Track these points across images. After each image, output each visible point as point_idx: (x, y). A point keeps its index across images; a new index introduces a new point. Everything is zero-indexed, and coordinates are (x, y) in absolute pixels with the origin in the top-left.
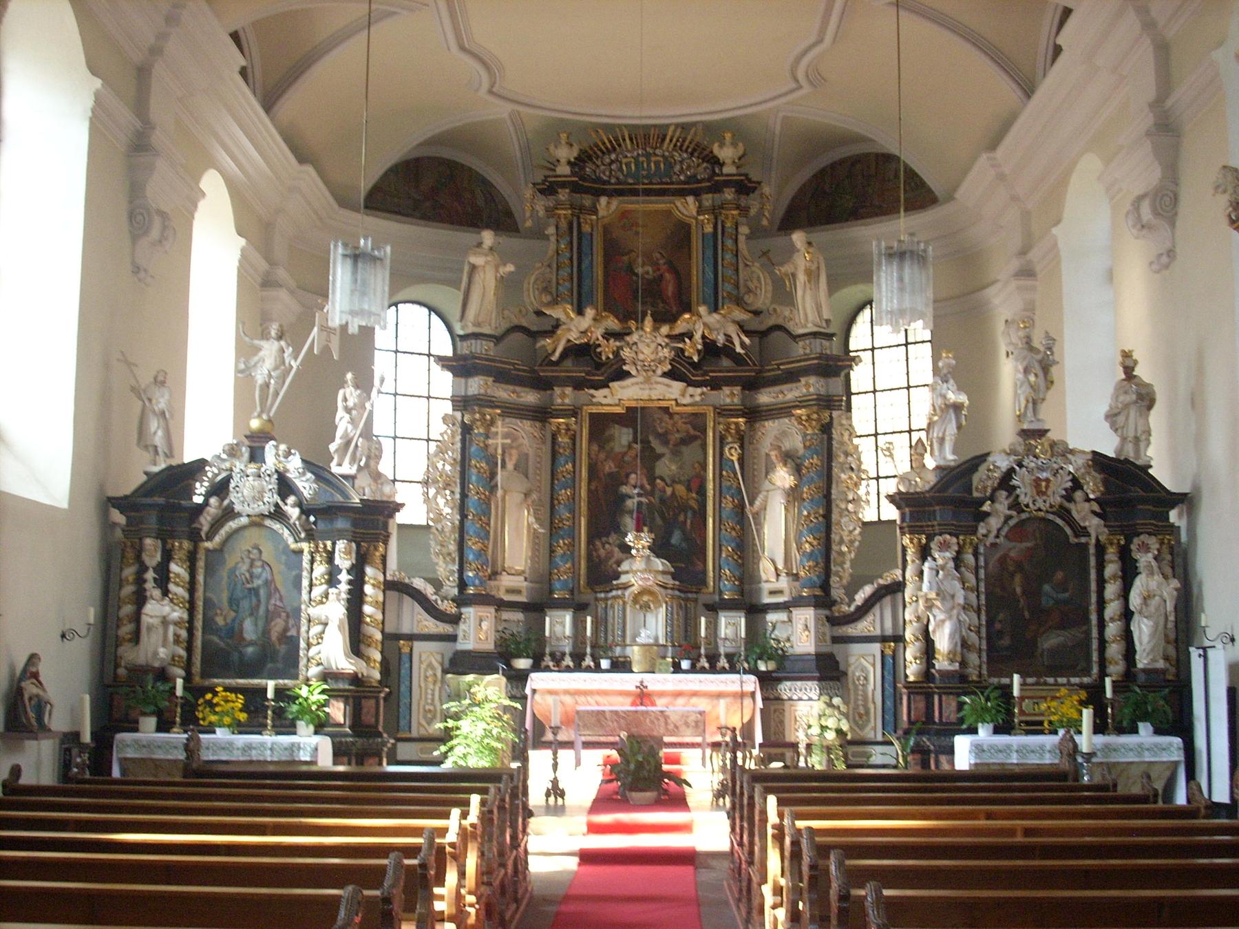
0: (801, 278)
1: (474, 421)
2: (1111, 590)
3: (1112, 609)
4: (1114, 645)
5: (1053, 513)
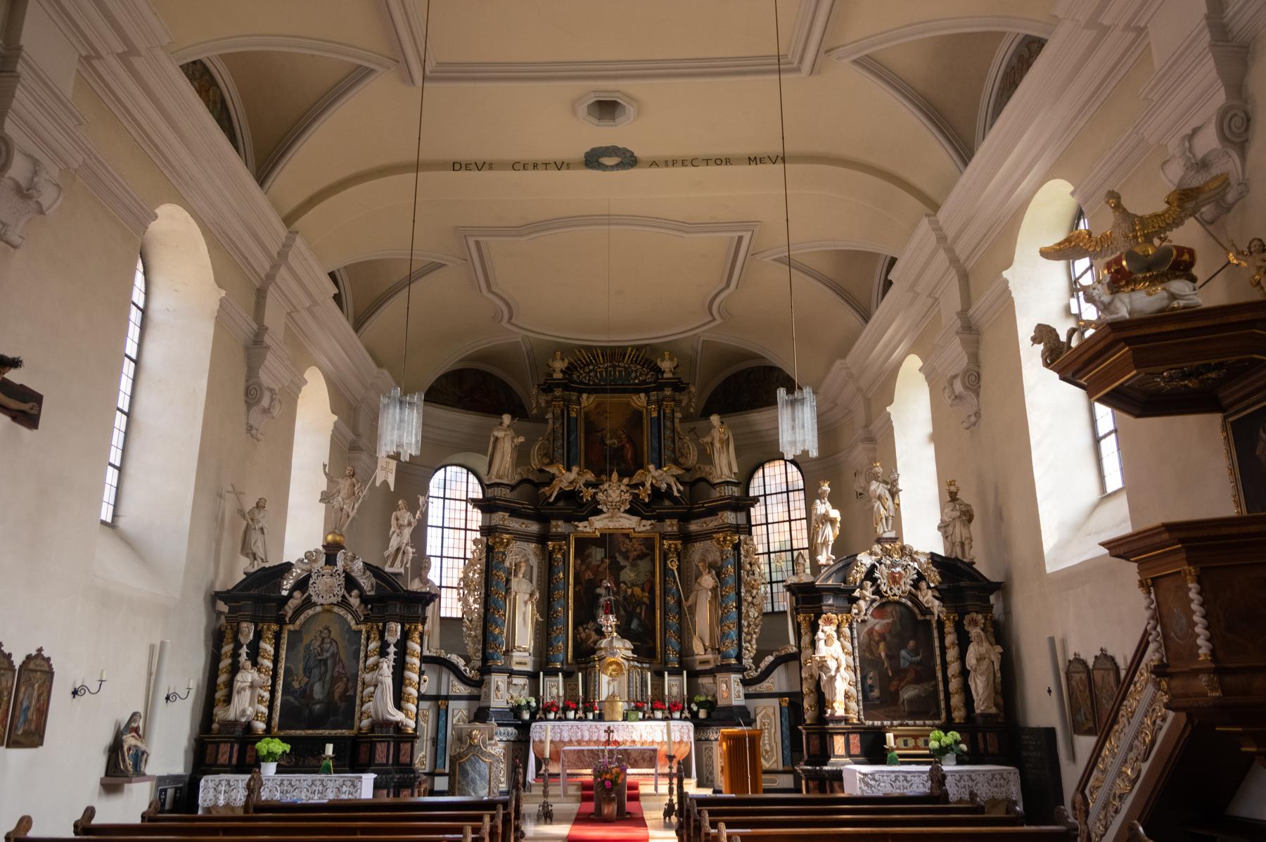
0: (717, 445)
1: (495, 543)
2: (952, 654)
3: (953, 668)
4: (956, 696)
5: (905, 598)
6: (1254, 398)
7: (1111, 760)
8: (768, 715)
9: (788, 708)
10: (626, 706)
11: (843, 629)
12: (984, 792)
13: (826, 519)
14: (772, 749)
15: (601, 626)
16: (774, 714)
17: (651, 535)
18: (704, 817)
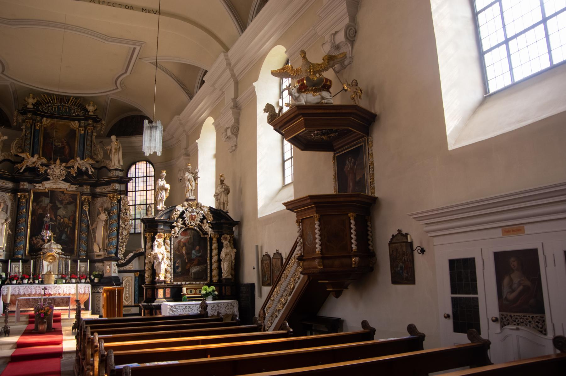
0: (113, 150)
2: (215, 252)
3: (215, 259)
4: (215, 271)
5: (196, 227)
6: (346, 147)
7: (277, 296)
8: (129, 281)
9: (139, 277)
10: (56, 277)
11: (167, 240)
12: (223, 311)
13: (163, 188)
14: (129, 296)
15: (43, 236)
16: (132, 280)
17: (75, 193)
18: (88, 330)
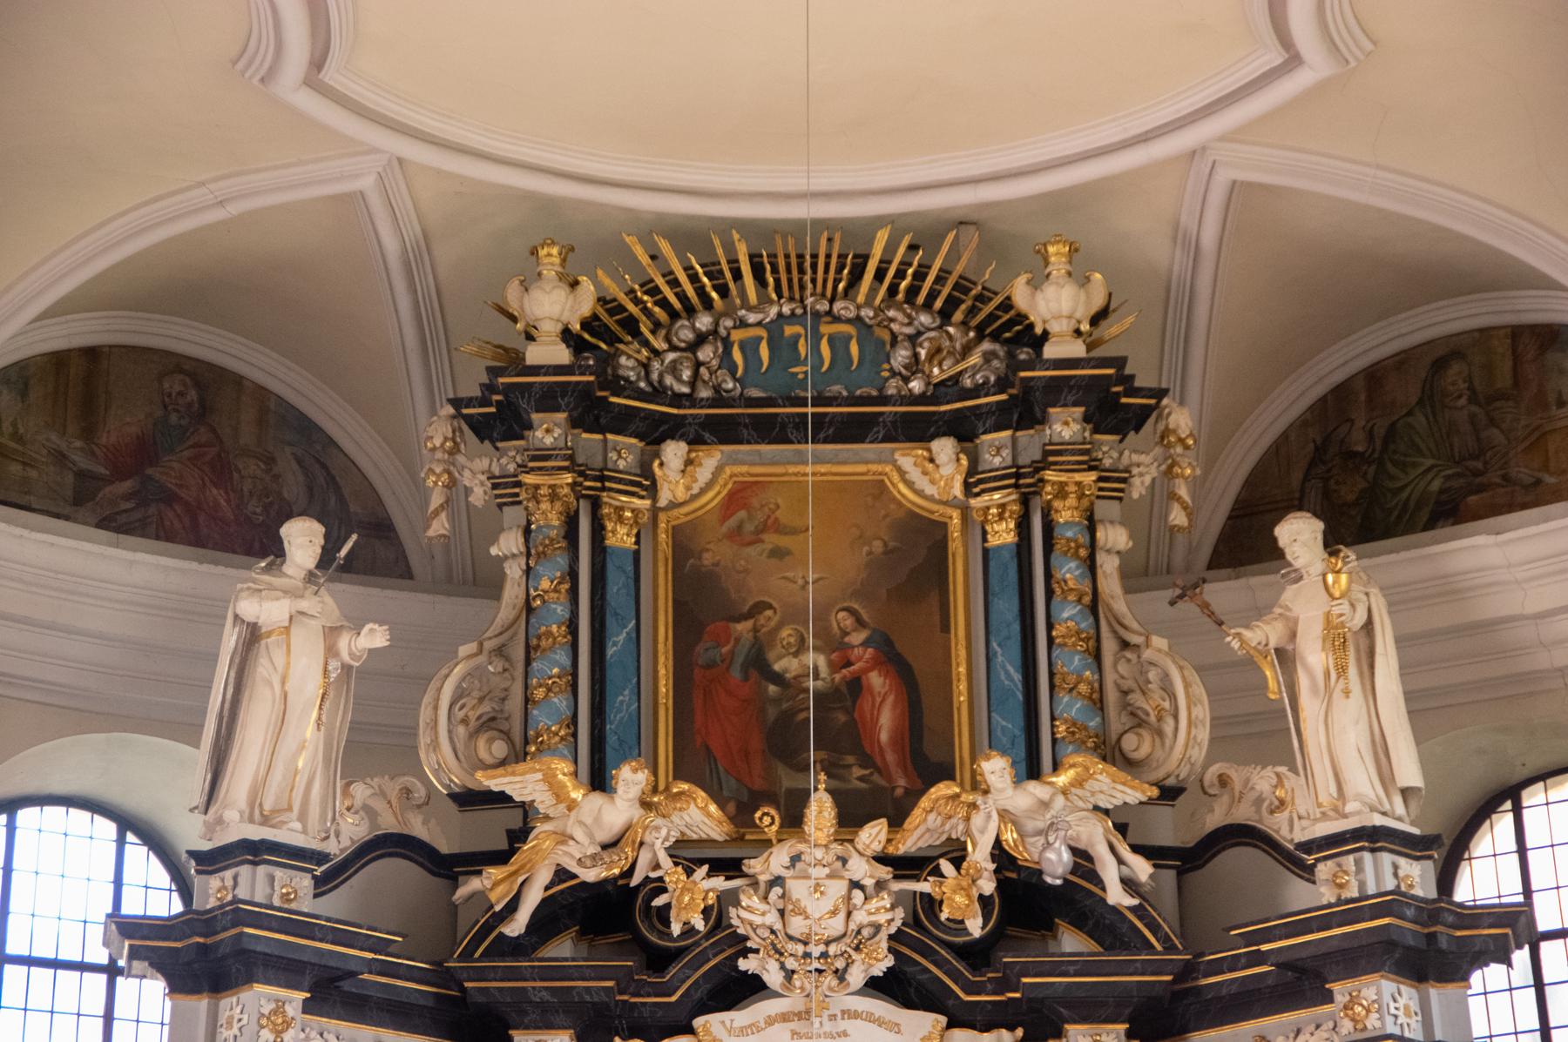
0: (1314, 657)
